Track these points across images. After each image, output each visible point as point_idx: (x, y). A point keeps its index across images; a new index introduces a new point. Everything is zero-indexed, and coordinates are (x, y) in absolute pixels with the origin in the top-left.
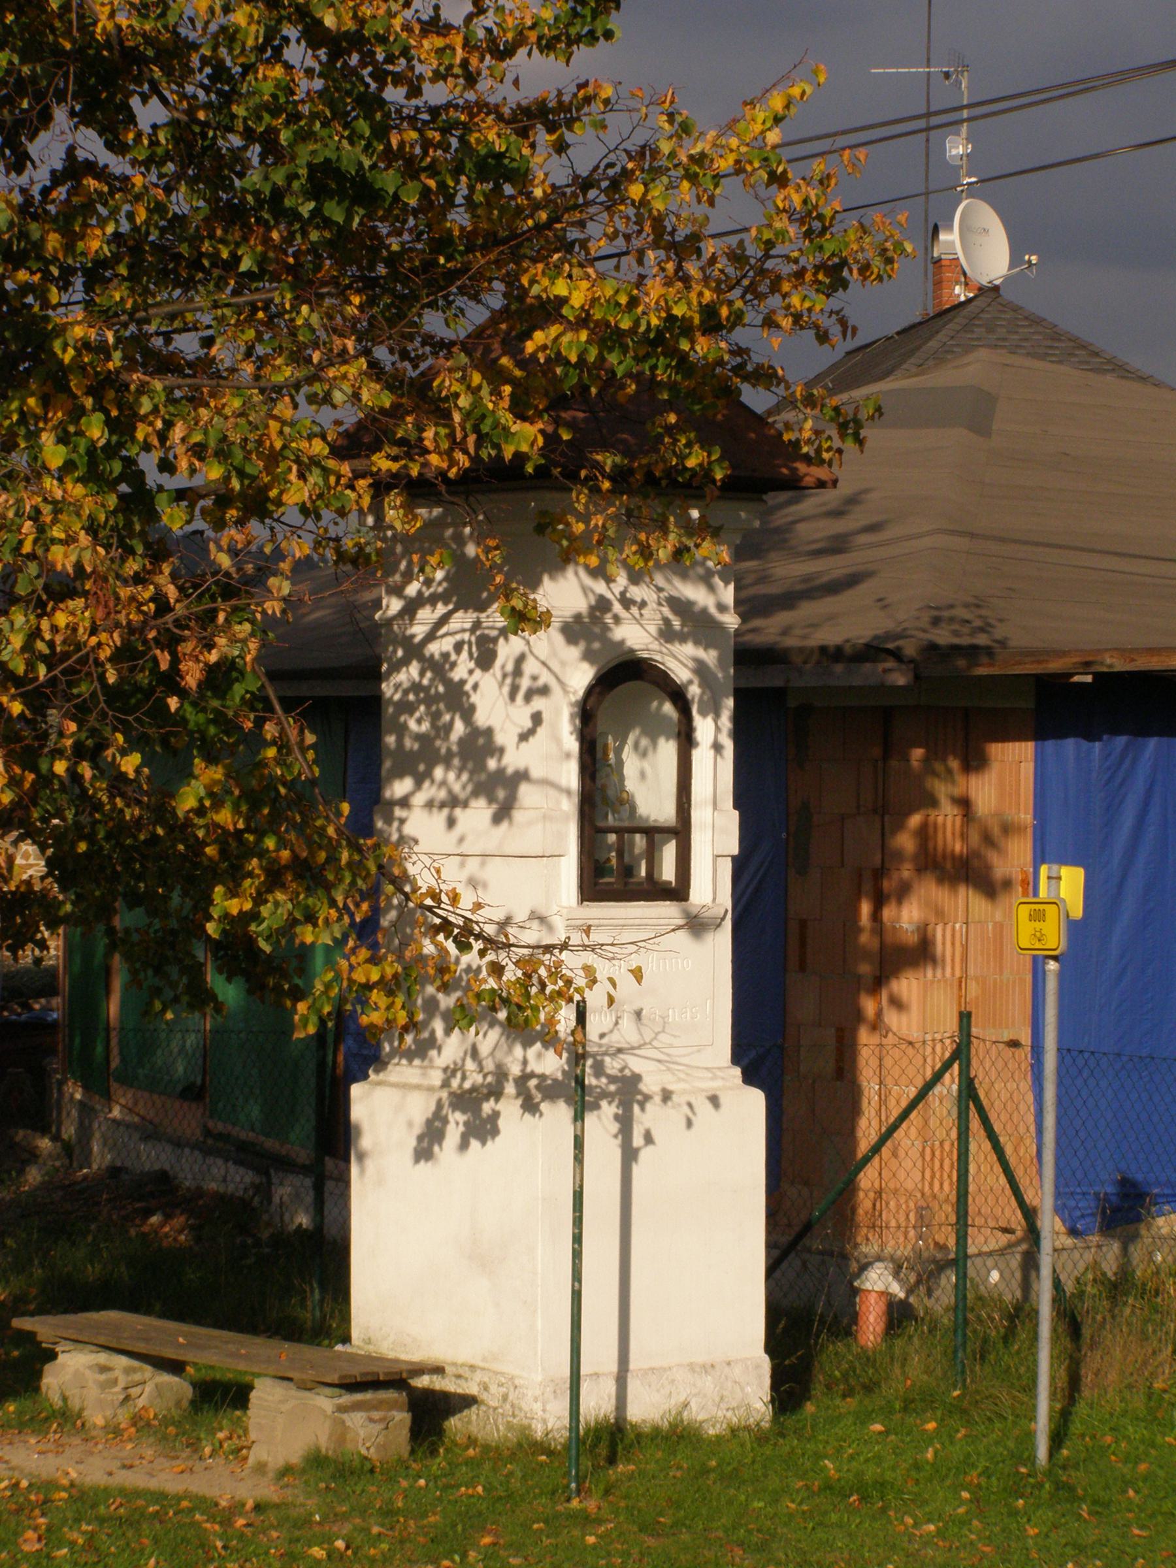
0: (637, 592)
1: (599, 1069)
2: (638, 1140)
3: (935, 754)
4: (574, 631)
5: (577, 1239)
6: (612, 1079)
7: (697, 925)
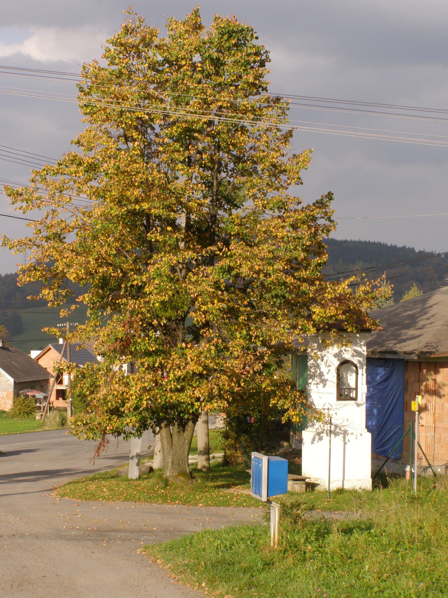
0: (347, 349)
1: (340, 429)
2: (347, 441)
3: (428, 371)
5: (330, 456)
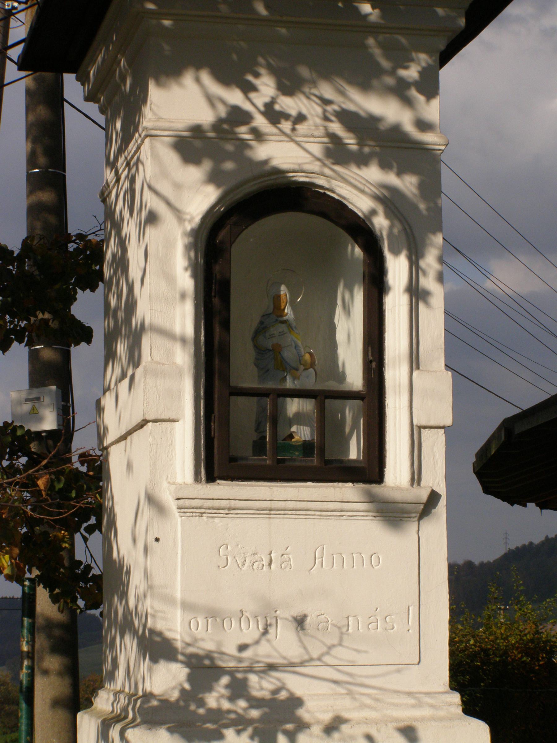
0: (289, 104)
4: (192, 145)
6: (255, 703)
7: (392, 514)
